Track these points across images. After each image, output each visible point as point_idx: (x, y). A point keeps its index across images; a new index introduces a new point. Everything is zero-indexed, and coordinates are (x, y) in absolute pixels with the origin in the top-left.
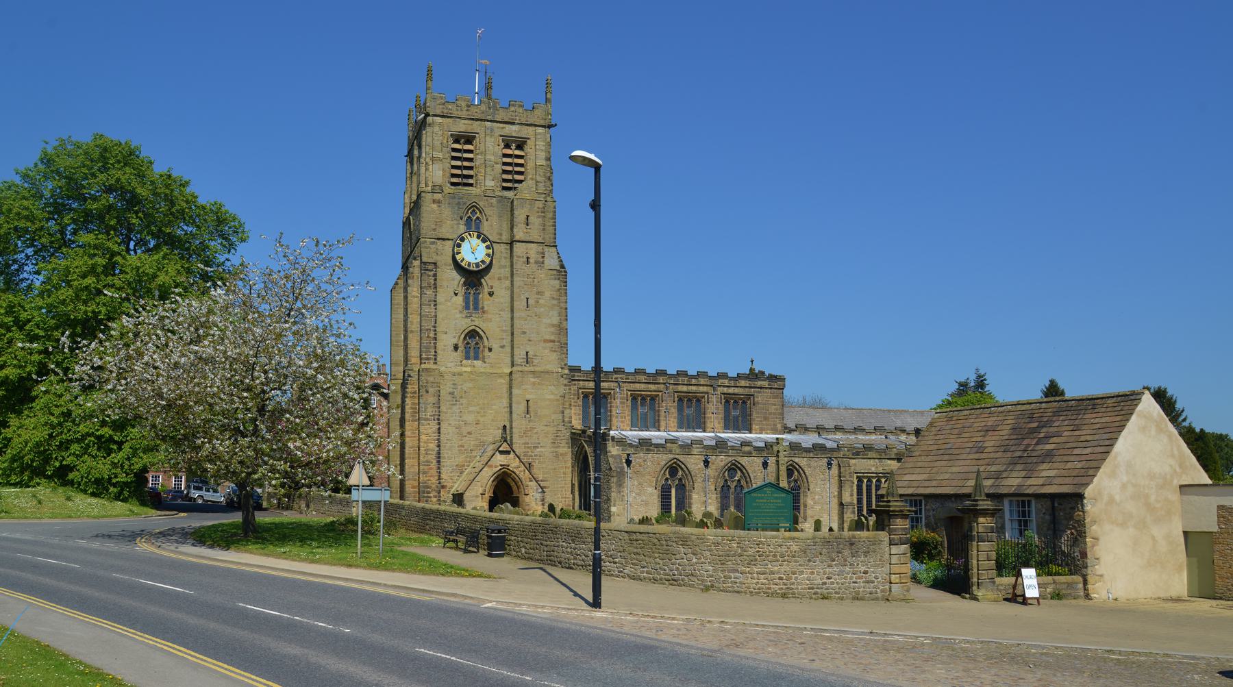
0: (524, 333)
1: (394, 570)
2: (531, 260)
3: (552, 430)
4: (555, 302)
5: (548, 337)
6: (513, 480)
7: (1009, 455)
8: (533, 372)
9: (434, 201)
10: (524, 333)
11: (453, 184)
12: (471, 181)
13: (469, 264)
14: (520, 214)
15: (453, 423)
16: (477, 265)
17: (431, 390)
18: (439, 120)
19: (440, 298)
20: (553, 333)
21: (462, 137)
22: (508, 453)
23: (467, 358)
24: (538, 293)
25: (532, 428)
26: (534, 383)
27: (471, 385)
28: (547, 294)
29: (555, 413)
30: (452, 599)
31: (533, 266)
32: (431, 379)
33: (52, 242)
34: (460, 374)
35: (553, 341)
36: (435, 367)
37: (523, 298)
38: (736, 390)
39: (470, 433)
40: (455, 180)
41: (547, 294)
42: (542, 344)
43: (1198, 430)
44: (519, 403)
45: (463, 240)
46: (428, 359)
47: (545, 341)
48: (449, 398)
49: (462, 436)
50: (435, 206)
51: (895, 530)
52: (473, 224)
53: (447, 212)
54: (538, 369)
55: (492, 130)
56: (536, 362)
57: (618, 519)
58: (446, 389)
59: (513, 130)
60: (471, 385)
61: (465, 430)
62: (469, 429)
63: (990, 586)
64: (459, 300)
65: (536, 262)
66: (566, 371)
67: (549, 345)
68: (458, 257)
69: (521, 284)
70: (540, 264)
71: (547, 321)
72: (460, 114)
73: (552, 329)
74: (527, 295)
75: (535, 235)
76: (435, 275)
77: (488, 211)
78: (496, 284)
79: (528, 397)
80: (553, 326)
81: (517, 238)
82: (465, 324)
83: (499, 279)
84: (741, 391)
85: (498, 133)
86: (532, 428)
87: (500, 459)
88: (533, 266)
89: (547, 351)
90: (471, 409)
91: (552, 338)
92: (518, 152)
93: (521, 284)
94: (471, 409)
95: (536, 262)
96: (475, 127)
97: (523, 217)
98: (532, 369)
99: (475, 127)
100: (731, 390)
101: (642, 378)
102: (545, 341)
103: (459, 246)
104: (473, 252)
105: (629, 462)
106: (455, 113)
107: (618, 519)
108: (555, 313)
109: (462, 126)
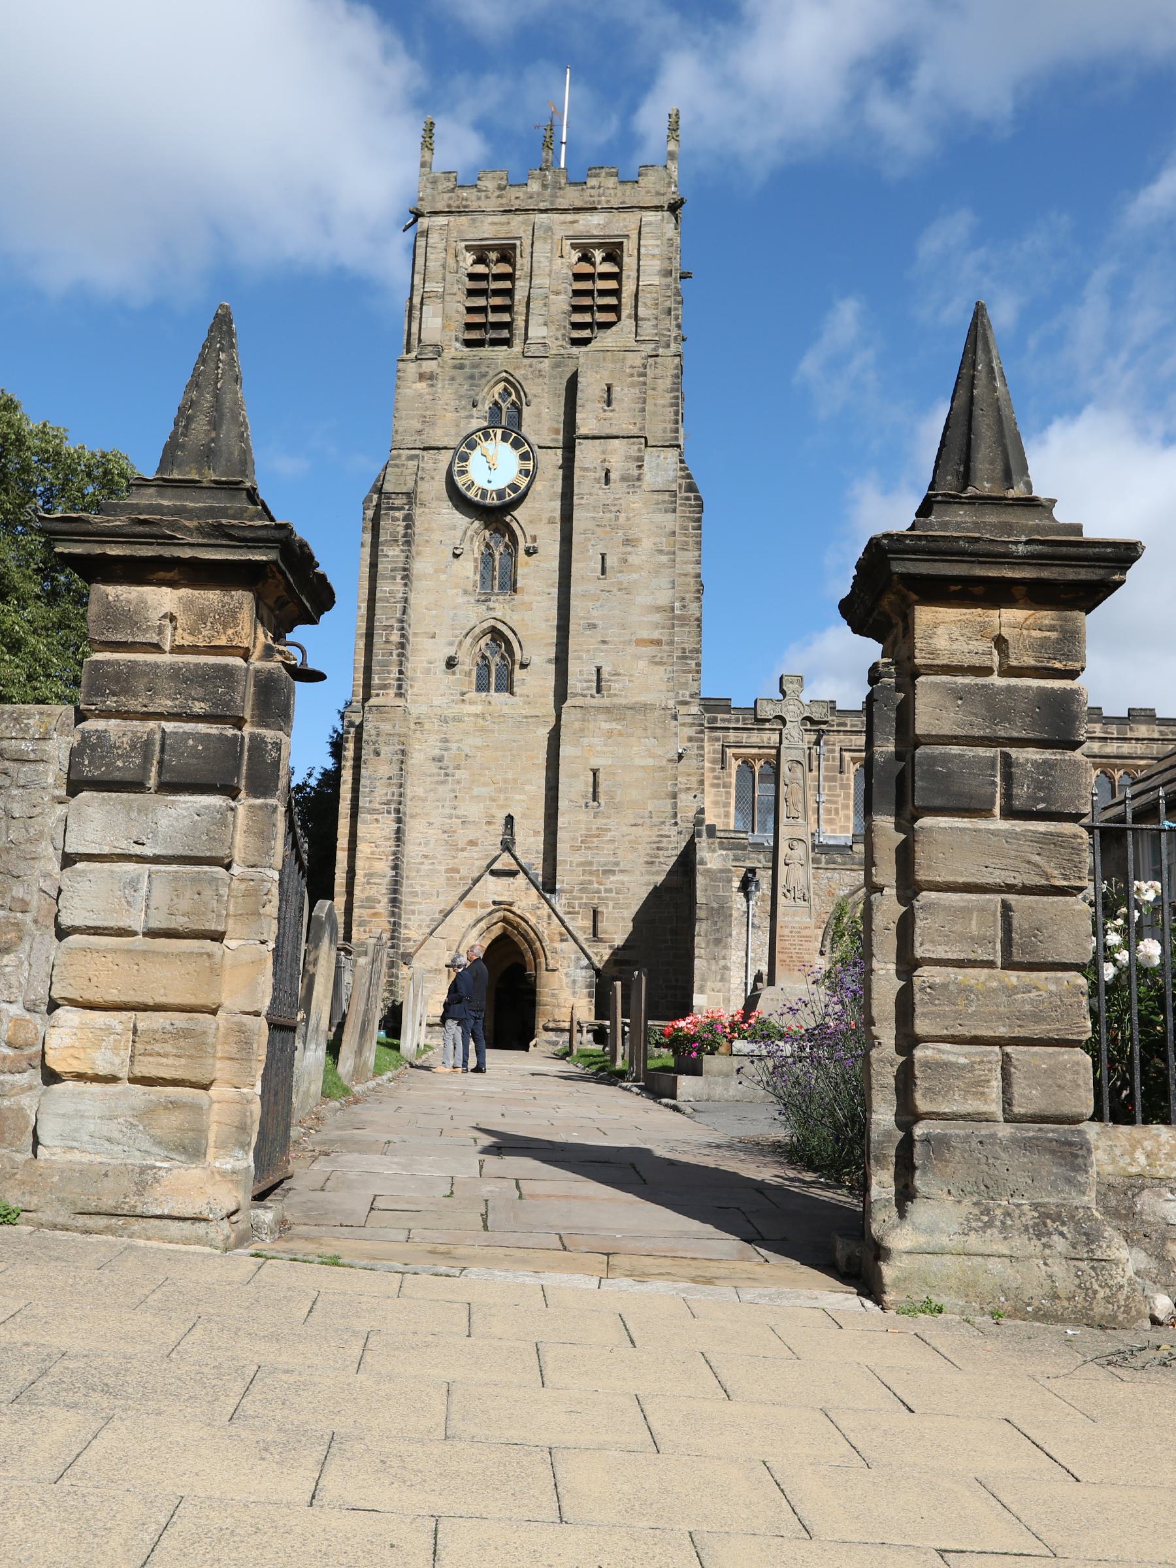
0: (593, 626)
2: (613, 476)
3: (646, 834)
4: (664, 559)
5: (645, 634)
8: (607, 709)
9: (422, 377)
10: (593, 626)
11: (468, 343)
13: (484, 493)
15: (437, 821)
16: (500, 494)
17: (385, 750)
18: (442, 220)
19: (419, 566)
20: (657, 626)
22: (512, 874)
23: (482, 687)
24: (627, 542)
25: (603, 830)
26: (610, 733)
27: (478, 741)
28: (647, 544)
32: (386, 727)
34: (458, 719)
35: (658, 643)
36: (399, 702)
38: (1126, 748)
39: (472, 843)
40: (475, 335)
41: (647, 544)
42: (632, 649)
44: (574, 776)
45: (472, 446)
46: (385, 687)
47: (640, 642)
48: (433, 768)
49: (455, 848)
50: (422, 386)
51: (123, 680)
52: (507, 421)
53: (447, 394)
55: (549, 229)
56: (616, 687)
58: (421, 754)
59: (592, 224)
60: (478, 741)
61: (463, 835)
62: (472, 833)
63: (1029, 1186)
64: (468, 568)
65: (624, 479)
66: (695, 709)
67: (651, 650)
68: (460, 481)
69: (591, 525)
70: (633, 481)
71: (644, 598)
72: (484, 204)
73: (657, 617)
75: (622, 419)
76: (408, 518)
77: (530, 388)
79: (595, 762)
80: (658, 609)
82: (475, 616)
84: (1140, 749)
85: (560, 232)
86: (603, 830)
87: (494, 889)
89: (642, 664)
90: (476, 791)
91: (656, 635)
93: (591, 525)
94: (476, 791)
95: (624, 479)
96: (517, 226)
98: (606, 701)
99: (517, 226)
100: (1112, 748)
102: (640, 642)
103: (464, 458)
104: (493, 468)
106: (474, 205)
108: (664, 582)
109: (488, 229)
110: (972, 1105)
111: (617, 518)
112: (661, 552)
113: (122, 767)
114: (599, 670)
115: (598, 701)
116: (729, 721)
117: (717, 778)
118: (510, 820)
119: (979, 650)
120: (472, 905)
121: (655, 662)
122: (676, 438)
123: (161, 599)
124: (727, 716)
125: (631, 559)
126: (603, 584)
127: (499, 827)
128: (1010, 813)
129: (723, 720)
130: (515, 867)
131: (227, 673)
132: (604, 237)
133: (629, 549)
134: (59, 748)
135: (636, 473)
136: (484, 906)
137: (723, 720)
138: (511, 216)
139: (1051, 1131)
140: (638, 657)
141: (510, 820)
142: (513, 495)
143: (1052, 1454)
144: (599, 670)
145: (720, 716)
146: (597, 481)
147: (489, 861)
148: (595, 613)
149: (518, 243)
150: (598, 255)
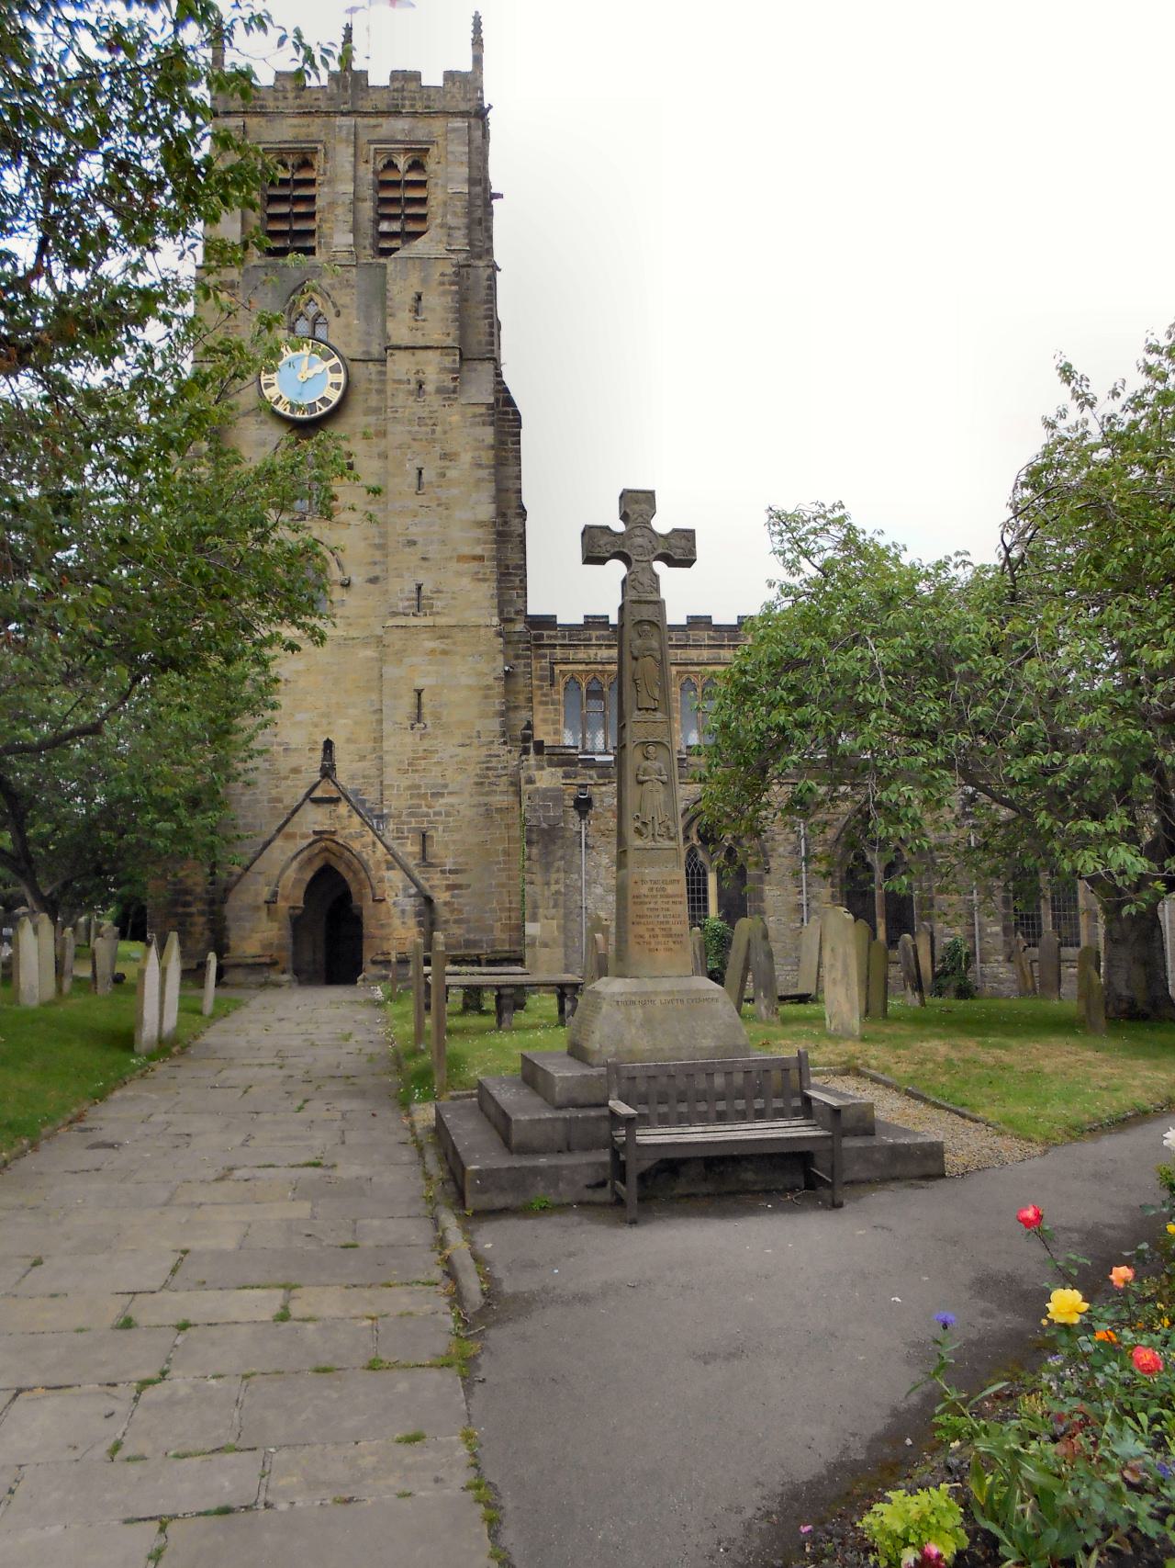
2: (429, 387)
4: (484, 473)
5: (466, 550)
6: (349, 865)
10: (412, 543)
12: (310, 243)
20: (478, 541)
21: (290, 152)
24: (444, 456)
28: (466, 458)
29: (483, 716)
31: (434, 401)
35: (481, 558)
37: (410, 468)
42: (454, 566)
43: (379, 78)
47: (461, 558)
54: (441, 621)
56: (438, 605)
57: (543, 954)
65: (439, 391)
67: (474, 566)
71: (463, 514)
73: (480, 533)
74: (418, 463)
79: (419, 683)
80: (481, 524)
81: (394, 341)
83: (366, 436)
87: (314, 819)
90: (299, 717)
91: (478, 551)
95: (439, 391)
97: (408, 298)
98: (428, 621)
101: (704, 636)
102: (461, 558)
107: (543, 954)
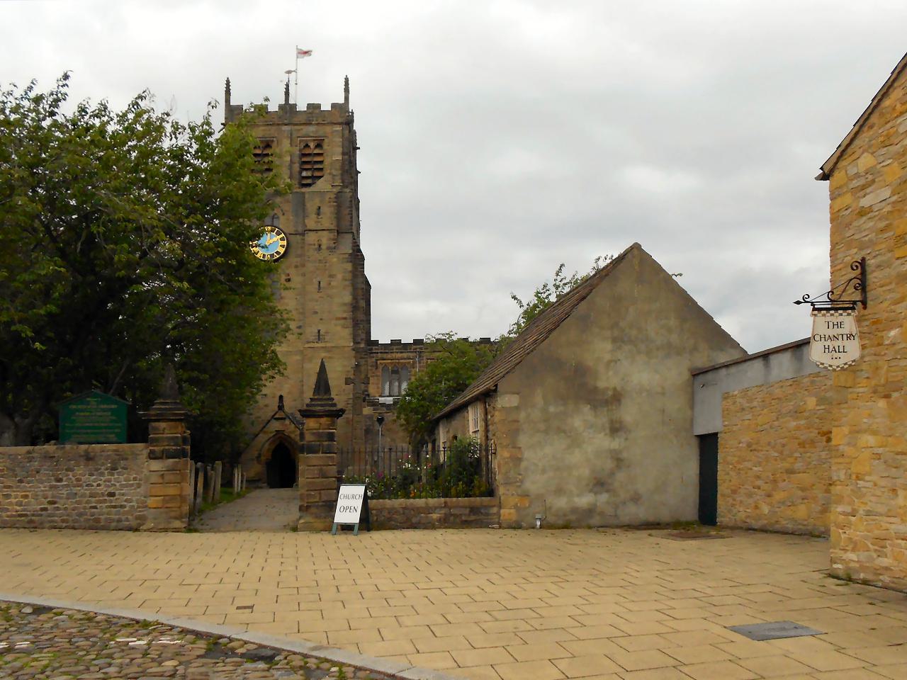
0: (316, 313)
1: (430, 526)
2: (324, 247)
5: (340, 315)
7: (877, 248)
10: (316, 313)
14: (311, 206)
20: (345, 312)
28: (339, 276)
30: (236, 482)
31: (325, 253)
33: (746, 473)
35: (345, 318)
47: (338, 319)
54: (328, 345)
56: (327, 338)
65: (328, 248)
67: (342, 322)
74: (319, 279)
78: (292, 272)
81: (308, 228)
88: (325, 253)
89: (339, 328)
91: (345, 315)
92: (317, 151)
102: (338, 319)
105: (380, 421)
110: (315, 500)
111: (325, 266)
112: (346, 280)
113: (158, 455)
114: (319, 331)
115: (320, 345)
116: (378, 349)
117: (374, 373)
118: (281, 397)
119: (316, 426)
120: (265, 433)
121: (344, 327)
122: (351, 229)
123: (163, 425)
124: (377, 347)
125: (332, 283)
126: (320, 295)
127: (277, 399)
128: (322, 453)
129: (376, 349)
130: (284, 416)
131: (177, 437)
132: (316, 137)
133: (331, 279)
134: (145, 452)
135: (334, 245)
136: (271, 433)
137: (376, 349)
138: (270, 127)
139: (328, 503)
140: (336, 325)
141: (281, 397)
142: (278, 256)
143: (642, 672)
144: (319, 331)
145: (374, 348)
146: (316, 249)
147: (274, 413)
148: (316, 307)
149: (274, 139)
150: (312, 145)
